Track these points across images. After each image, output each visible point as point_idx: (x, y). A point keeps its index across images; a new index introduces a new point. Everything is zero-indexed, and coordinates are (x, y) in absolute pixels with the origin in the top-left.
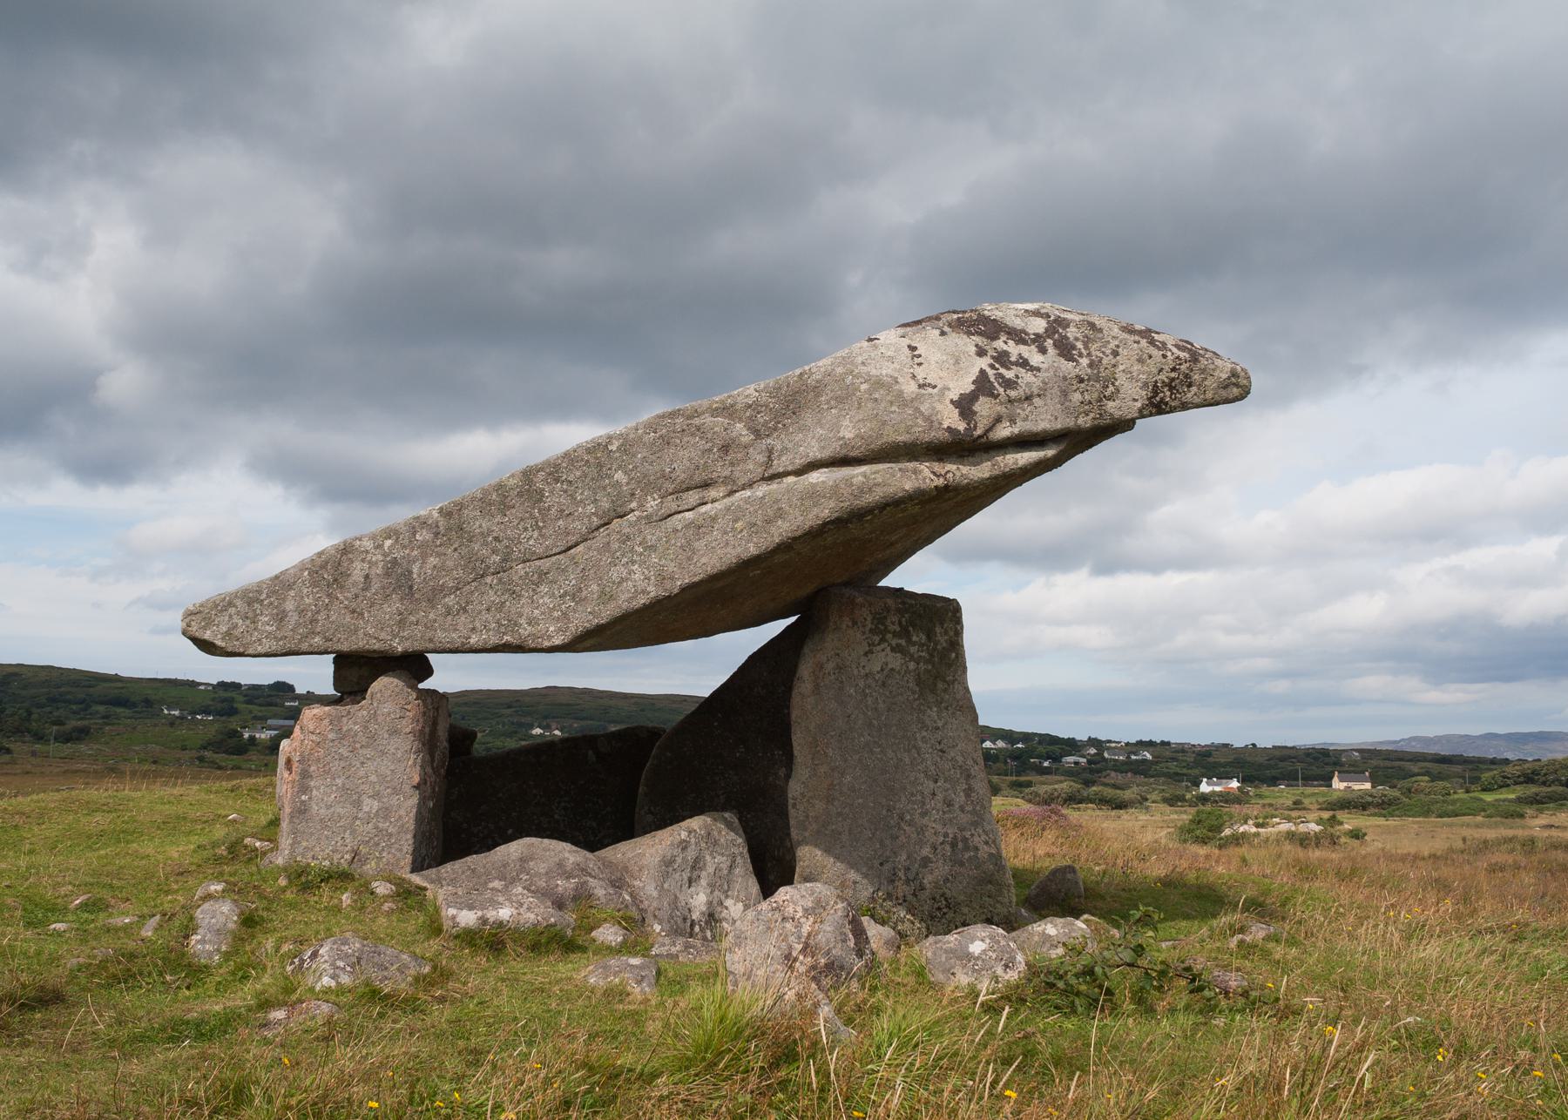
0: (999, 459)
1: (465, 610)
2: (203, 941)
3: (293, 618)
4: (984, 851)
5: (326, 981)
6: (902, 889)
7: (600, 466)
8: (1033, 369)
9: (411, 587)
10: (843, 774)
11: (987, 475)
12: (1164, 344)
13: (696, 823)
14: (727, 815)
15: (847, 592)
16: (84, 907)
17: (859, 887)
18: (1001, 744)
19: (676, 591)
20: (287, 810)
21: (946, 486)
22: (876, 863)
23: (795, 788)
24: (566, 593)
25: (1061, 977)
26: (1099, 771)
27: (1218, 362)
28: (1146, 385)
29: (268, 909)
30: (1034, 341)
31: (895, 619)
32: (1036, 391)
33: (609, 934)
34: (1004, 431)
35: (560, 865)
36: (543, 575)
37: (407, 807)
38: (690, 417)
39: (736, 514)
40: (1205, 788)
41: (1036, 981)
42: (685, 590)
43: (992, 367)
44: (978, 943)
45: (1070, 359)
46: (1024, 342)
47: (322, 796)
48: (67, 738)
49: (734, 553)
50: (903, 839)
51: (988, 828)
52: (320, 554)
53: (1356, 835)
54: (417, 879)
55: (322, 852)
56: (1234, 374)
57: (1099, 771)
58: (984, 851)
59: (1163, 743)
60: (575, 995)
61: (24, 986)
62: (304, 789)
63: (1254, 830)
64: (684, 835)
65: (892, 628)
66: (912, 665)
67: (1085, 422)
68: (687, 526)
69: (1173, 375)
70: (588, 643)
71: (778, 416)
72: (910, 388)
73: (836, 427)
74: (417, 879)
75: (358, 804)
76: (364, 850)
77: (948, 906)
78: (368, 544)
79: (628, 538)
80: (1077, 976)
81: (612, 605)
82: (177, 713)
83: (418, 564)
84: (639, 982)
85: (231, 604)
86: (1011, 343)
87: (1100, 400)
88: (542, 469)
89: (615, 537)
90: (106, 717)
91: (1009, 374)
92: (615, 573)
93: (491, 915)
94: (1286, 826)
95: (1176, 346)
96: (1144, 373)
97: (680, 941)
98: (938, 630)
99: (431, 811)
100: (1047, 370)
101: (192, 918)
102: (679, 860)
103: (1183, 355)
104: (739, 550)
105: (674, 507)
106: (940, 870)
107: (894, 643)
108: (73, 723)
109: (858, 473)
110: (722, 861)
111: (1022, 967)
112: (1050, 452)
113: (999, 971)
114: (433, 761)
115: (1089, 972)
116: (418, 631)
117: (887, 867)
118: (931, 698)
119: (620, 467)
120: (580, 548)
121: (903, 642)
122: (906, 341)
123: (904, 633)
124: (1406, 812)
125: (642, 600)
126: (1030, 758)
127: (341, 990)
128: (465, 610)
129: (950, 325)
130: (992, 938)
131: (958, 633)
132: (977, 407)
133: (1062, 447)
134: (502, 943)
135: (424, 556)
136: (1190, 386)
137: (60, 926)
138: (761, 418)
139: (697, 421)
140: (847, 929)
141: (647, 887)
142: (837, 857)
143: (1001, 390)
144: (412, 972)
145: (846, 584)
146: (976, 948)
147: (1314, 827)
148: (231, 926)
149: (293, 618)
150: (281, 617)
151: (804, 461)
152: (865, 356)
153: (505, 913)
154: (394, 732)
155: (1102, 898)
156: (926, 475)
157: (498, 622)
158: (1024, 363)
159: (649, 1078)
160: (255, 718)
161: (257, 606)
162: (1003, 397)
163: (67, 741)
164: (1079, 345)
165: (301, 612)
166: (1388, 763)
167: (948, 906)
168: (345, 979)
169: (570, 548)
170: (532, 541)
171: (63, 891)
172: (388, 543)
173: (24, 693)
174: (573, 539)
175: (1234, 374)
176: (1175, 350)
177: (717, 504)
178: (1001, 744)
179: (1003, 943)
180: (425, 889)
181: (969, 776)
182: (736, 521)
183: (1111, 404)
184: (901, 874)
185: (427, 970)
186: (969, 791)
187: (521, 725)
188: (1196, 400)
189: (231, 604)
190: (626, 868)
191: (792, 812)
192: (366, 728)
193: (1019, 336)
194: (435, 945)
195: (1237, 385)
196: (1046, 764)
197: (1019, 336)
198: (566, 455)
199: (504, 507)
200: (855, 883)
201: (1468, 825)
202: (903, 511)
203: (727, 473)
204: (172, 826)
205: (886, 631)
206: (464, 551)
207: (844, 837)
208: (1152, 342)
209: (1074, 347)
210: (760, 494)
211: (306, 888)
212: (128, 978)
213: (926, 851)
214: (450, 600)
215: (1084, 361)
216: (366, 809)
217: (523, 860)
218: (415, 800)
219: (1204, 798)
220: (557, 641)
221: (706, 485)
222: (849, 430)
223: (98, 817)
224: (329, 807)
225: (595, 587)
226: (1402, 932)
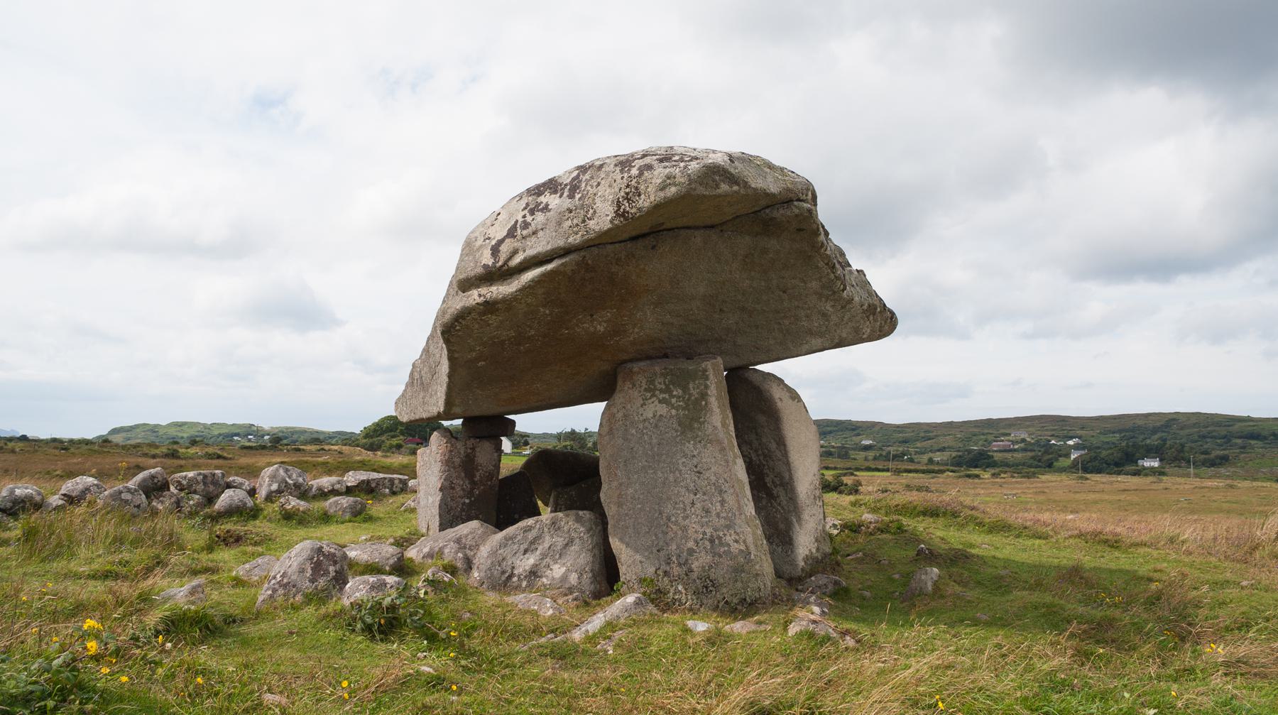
4: (735, 548)
6: (676, 570)
22: (655, 550)
31: (661, 380)
34: (518, 259)
50: (671, 534)
58: (735, 548)
66: (674, 412)
87: (584, 221)
90: (1244, 447)
98: (691, 386)
107: (661, 396)
117: (662, 554)
158: (546, 208)
173: (1182, 433)
181: (721, 492)
184: (674, 559)
186: (723, 502)
207: (630, 530)
213: (691, 544)
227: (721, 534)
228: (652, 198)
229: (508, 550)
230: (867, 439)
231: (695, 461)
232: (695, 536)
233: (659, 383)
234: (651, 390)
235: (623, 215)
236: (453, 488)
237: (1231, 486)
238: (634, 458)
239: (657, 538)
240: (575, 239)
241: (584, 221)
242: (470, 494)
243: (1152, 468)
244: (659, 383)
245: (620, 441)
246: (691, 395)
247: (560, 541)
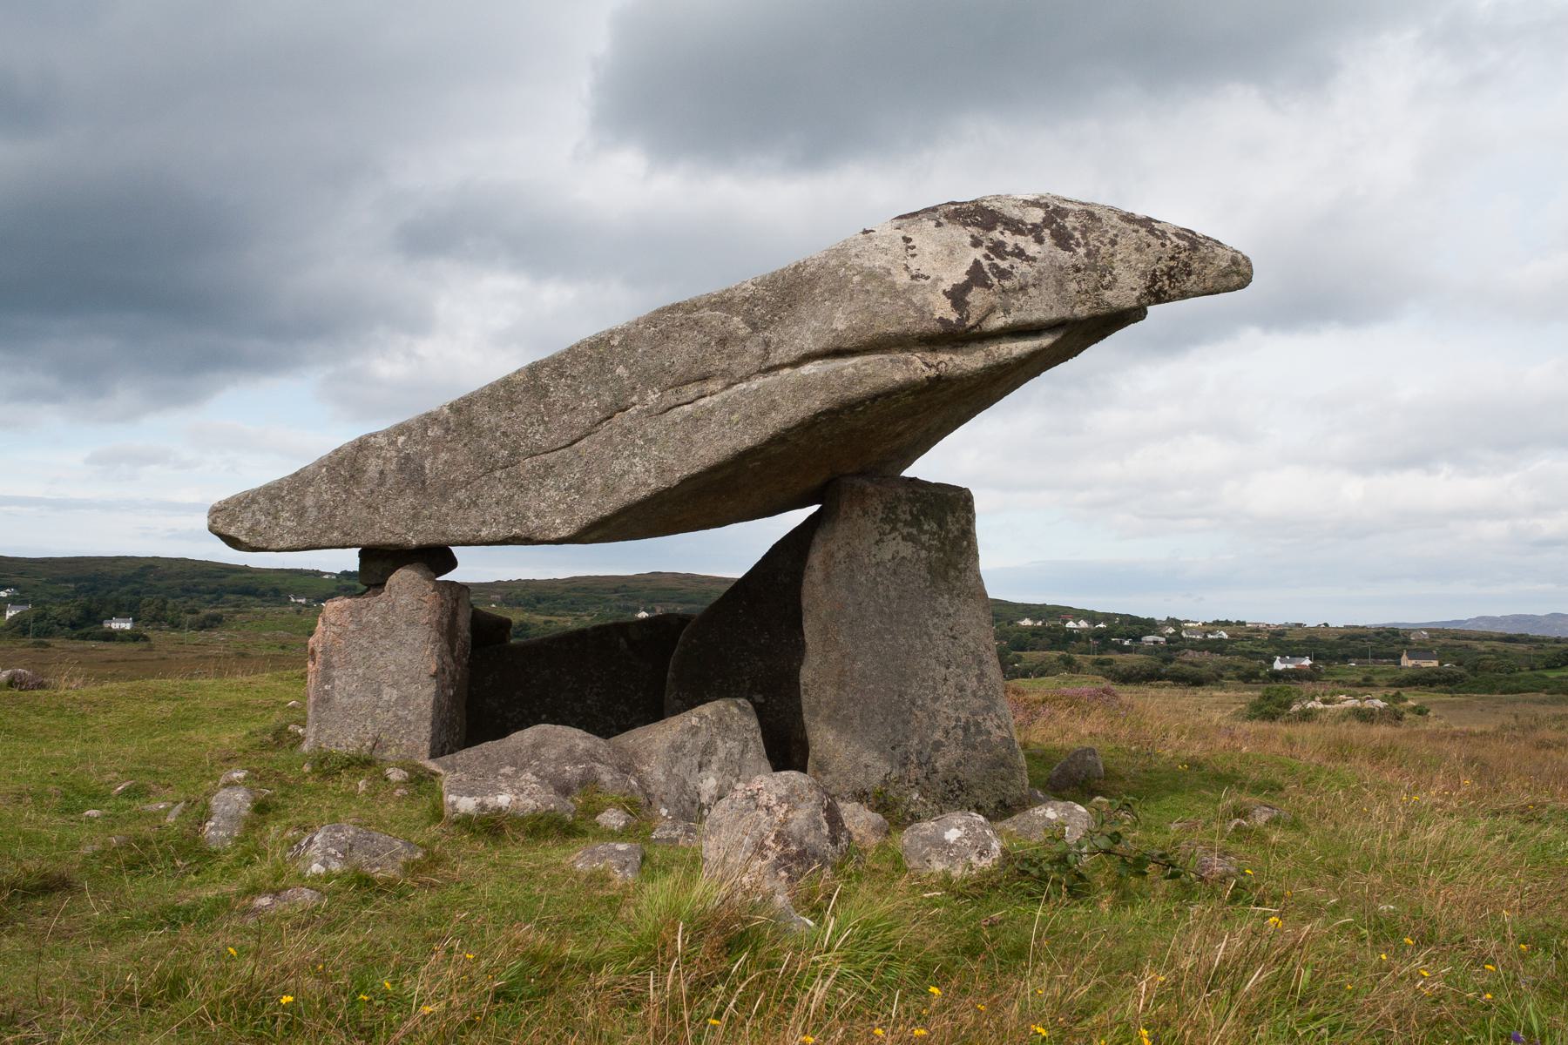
0: (993, 348)
1: (476, 505)
2: (216, 828)
3: (313, 513)
4: (997, 735)
5: (316, 868)
6: (915, 772)
7: (602, 360)
8: (1031, 259)
9: (424, 482)
11: (980, 365)
12: (1163, 232)
13: (707, 709)
14: (741, 701)
15: (858, 482)
16: (127, 793)
17: (871, 770)
18: (1083, 624)
19: (676, 483)
20: (312, 699)
21: (939, 377)
22: (888, 748)
23: (806, 675)
24: (571, 486)
25: (1035, 865)
26: (1178, 650)
27: (1219, 250)
28: (1144, 273)
29: (283, 795)
30: (1031, 231)
31: (907, 508)
32: (1031, 281)
33: (612, 818)
34: (997, 322)
35: (570, 751)
36: (549, 468)
37: (424, 695)
38: (689, 312)
39: (731, 406)
40: (1278, 665)
41: (1010, 868)
42: (684, 482)
43: (987, 257)
44: (954, 830)
45: (1067, 248)
46: (1020, 232)
47: (344, 685)
48: (203, 626)
49: (730, 445)
50: (914, 723)
51: (1000, 712)
52: (337, 451)
53: (1420, 711)
54: (432, 765)
55: (348, 742)
56: (1234, 261)
57: (1178, 650)
58: (997, 735)
59: (1239, 623)
60: (560, 879)
61: (29, 875)
62: (327, 679)
63: (1321, 706)
64: (695, 721)
65: (903, 517)
66: (923, 554)
67: (1082, 311)
68: (685, 419)
69: (1172, 263)
70: (592, 536)
71: (774, 309)
72: (902, 279)
73: (829, 319)
74: (432, 765)
75: (378, 693)
76: (384, 737)
77: (961, 788)
78: (383, 441)
79: (630, 432)
80: (1051, 863)
81: (615, 497)
83: (429, 460)
84: (622, 868)
85: (254, 501)
86: (1007, 233)
87: (1097, 289)
88: (546, 365)
89: (617, 430)
91: (1004, 265)
92: (617, 466)
93: (490, 801)
94: (1351, 703)
95: (1177, 235)
96: (1141, 262)
97: (682, 825)
98: (949, 519)
99: (452, 699)
100: (1043, 260)
101: (207, 806)
102: (689, 745)
103: (1182, 243)
104: (735, 442)
105: (673, 401)
106: (952, 753)
107: (905, 531)
108: (207, 611)
109: (848, 365)
110: (734, 746)
111: (997, 854)
112: (1046, 341)
113: (974, 859)
114: (452, 651)
115: (1063, 859)
116: (431, 525)
117: (898, 751)
118: (943, 586)
119: (621, 362)
120: (584, 442)
121: (914, 531)
122: (902, 233)
123: (915, 522)
124: (1472, 688)
125: (643, 493)
126: (1045, 641)
127: (329, 877)
128: (476, 505)
129: (946, 217)
130: (968, 825)
131: (970, 521)
132: (969, 298)
133: (1058, 336)
134: (501, 828)
135: (436, 452)
136: (1189, 274)
137: (93, 813)
138: (758, 311)
139: (695, 315)
140: (822, 816)
141: (655, 772)
143: (995, 280)
144: (403, 859)
145: (862, 473)
146: (952, 835)
147: (1379, 703)
148: (244, 812)
149: (313, 513)
150: (301, 513)
151: (799, 353)
152: (860, 248)
153: (504, 800)
154: (411, 623)
155: (1122, 778)
156: (917, 366)
157: (507, 515)
158: (1020, 253)
159: (590, 967)
161: (278, 502)
163: (202, 628)
164: (1077, 235)
165: (321, 508)
166: (1456, 642)
167: (961, 788)
168: (336, 867)
169: (574, 442)
170: (538, 435)
171: (107, 778)
172: (401, 439)
174: (577, 433)
175: (1234, 261)
176: (1174, 239)
177: (715, 397)
178: (1083, 624)
179: (979, 830)
180: (437, 775)
181: (981, 662)
182: (732, 413)
184: (913, 758)
185: (419, 855)
186: (981, 677)
187: (627, 609)
188: (1196, 289)
189: (254, 501)
190: (635, 753)
191: (804, 698)
192: (385, 619)
193: (1016, 227)
194: (435, 830)
195: (1238, 273)
196: (1126, 643)
197: (1016, 227)
198: (570, 351)
199: (511, 402)
201: (1533, 701)
202: (897, 401)
203: (724, 366)
204: (231, 713)
205: (897, 520)
206: (474, 446)
207: (856, 722)
208: (1152, 231)
209: (1072, 237)
210: (754, 386)
211: (327, 775)
212: (136, 866)
213: (938, 735)
214: (461, 494)
215: (1082, 251)
216: (386, 697)
217: (536, 746)
218: (432, 689)
219: (1277, 676)
220: (563, 533)
221: (704, 378)
222: (842, 321)
223: (164, 705)
224: (350, 696)
225: (598, 480)
226: (1429, 810)
227: (980, 719)
231: (950, 622)
232: (945, 723)
234: (891, 520)
239: (894, 730)
243: (123, 631)
246: (948, 532)
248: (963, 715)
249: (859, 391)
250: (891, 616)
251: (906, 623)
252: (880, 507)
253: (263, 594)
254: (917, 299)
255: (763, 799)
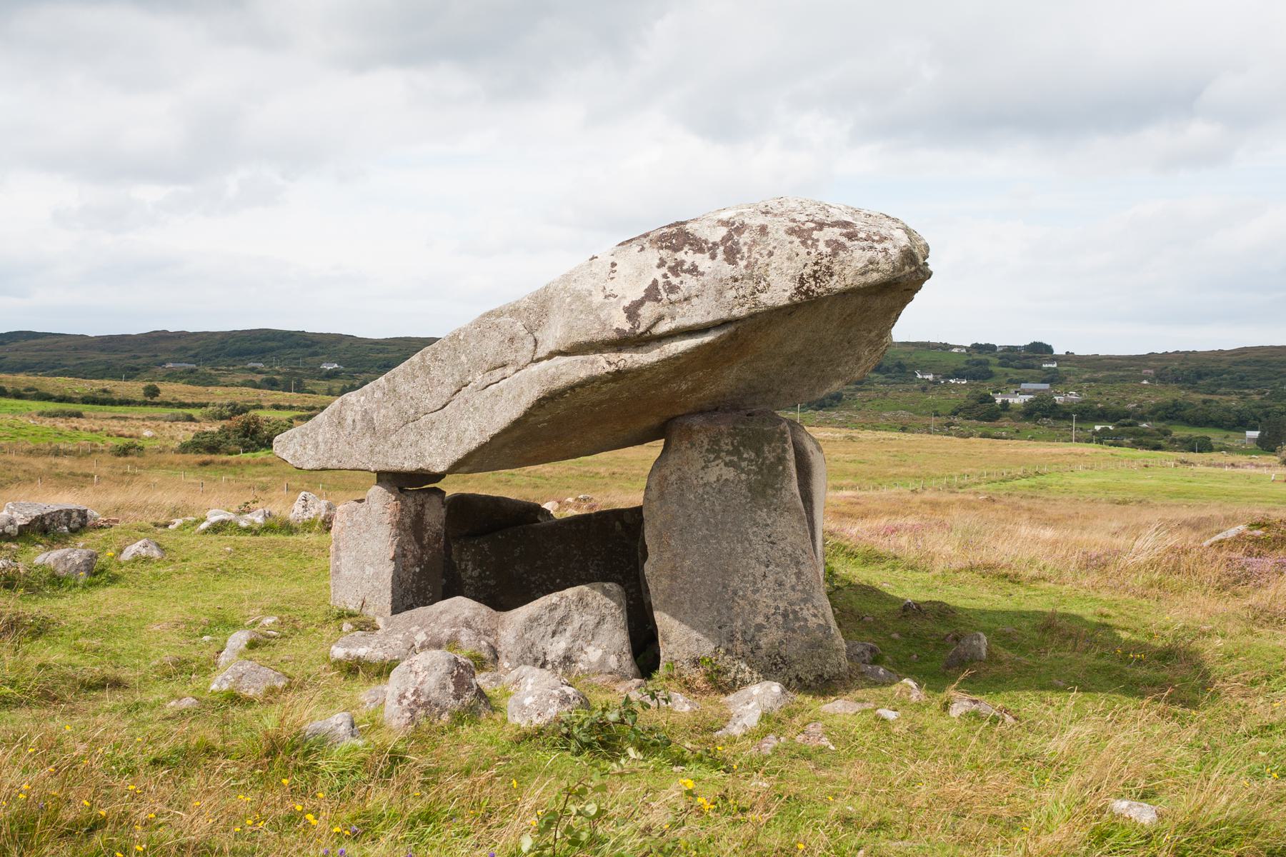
3: (322, 446)
4: (813, 622)
6: (740, 647)
10: (683, 559)
11: (655, 359)
13: (569, 592)
21: (618, 371)
22: (715, 627)
23: (648, 568)
28: (794, 277)
31: (728, 441)
32: (694, 293)
34: (663, 327)
58: (813, 622)
62: (338, 558)
65: (725, 448)
66: (743, 476)
69: (816, 268)
75: (363, 569)
77: (784, 662)
82: (930, 377)
87: (753, 293)
96: (793, 268)
98: (766, 449)
102: (545, 618)
107: (727, 459)
113: (534, 717)
117: (724, 630)
121: (735, 459)
136: (831, 275)
142: (682, 621)
143: (664, 295)
154: (381, 523)
158: (694, 270)
160: (1011, 382)
162: (665, 301)
164: (745, 249)
174: (445, 400)
181: (798, 563)
183: (763, 295)
184: (738, 635)
186: (799, 575)
197: (698, 246)
200: (698, 640)
205: (721, 450)
207: (687, 606)
214: (393, 438)
215: (742, 263)
218: (392, 568)
221: (504, 366)
227: (797, 608)
228: (849, 282)
229: (534, 633)
230: (330, 361)
231: (768, 530)
233: (726, 443)
234: (715, 449)
235: (806, 293)
236: (405, 556)
237: (851, 438)
238: (692, 526)
239: (720, 613)
240: (738, 312)
241: (753, 293)
242: (419, 561)
244: (726, 443)
245: (675, 507)
247: (591, 620)
248: (782, 605)
249: (560, 384)
250: (716, 525)
251: (730, 531)
252: (706, 442)
253: (888, 370)
254: (603, 315)
255: (415, 667)
